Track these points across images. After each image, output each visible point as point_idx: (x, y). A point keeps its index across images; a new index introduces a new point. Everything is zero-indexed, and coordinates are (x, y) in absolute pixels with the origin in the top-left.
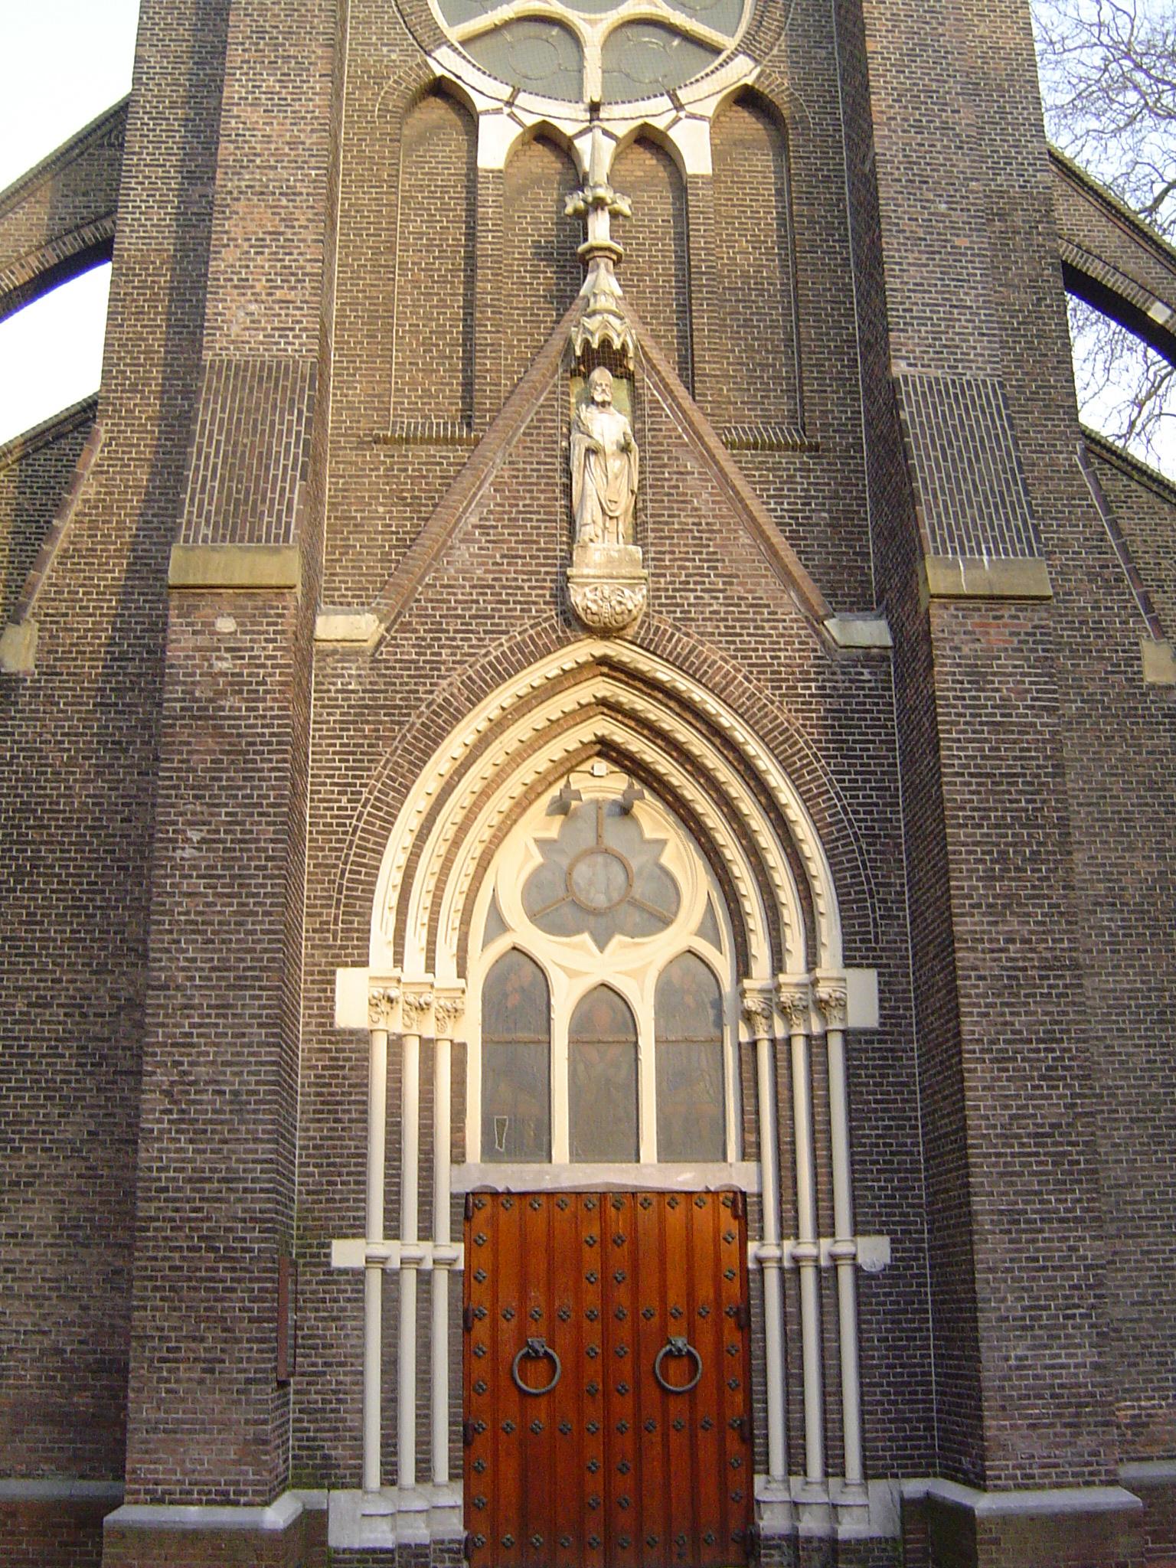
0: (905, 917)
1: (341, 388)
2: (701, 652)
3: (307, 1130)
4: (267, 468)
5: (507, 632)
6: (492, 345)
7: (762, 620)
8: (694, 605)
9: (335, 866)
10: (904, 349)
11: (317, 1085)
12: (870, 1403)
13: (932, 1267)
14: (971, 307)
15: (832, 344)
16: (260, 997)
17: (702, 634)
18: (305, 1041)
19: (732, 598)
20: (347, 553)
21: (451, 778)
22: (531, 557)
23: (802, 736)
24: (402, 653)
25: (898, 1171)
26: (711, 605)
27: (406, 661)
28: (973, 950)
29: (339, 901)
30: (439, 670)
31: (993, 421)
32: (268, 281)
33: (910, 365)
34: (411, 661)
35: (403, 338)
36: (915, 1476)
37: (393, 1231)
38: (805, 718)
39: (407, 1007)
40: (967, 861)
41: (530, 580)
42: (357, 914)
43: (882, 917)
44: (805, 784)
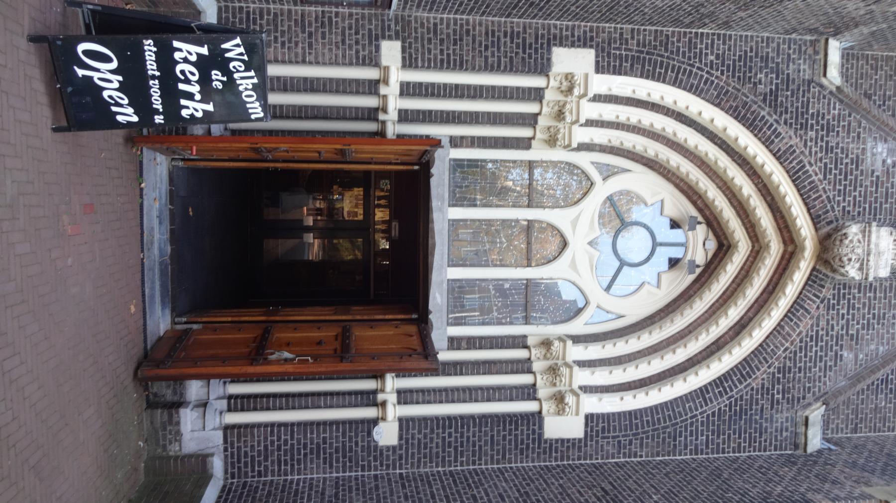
0: (619, 458)
2: (806, 318)
3: (480, 25)
5: (825, 178)
7: (826, 361)
8: (838, 314)
11: (512, 32)
12: (279, 431)
13: (376, 476)
17: (818, 318)
18: (543, 25)
19: (842, 340)
20: (872, 69)
21: (720, 138)
22: (876, 198)
23: (745, 387)
24: (814, 103)
25: (444, 451)
26: (838, 325)
29: (642, 52)
30: (801, 129)
36: (226, 463)
37: (407, 90)
39: (561, 104)
41: (860, 196)
42: (632, 65)
43: (619, 442)
44: (713, 390)
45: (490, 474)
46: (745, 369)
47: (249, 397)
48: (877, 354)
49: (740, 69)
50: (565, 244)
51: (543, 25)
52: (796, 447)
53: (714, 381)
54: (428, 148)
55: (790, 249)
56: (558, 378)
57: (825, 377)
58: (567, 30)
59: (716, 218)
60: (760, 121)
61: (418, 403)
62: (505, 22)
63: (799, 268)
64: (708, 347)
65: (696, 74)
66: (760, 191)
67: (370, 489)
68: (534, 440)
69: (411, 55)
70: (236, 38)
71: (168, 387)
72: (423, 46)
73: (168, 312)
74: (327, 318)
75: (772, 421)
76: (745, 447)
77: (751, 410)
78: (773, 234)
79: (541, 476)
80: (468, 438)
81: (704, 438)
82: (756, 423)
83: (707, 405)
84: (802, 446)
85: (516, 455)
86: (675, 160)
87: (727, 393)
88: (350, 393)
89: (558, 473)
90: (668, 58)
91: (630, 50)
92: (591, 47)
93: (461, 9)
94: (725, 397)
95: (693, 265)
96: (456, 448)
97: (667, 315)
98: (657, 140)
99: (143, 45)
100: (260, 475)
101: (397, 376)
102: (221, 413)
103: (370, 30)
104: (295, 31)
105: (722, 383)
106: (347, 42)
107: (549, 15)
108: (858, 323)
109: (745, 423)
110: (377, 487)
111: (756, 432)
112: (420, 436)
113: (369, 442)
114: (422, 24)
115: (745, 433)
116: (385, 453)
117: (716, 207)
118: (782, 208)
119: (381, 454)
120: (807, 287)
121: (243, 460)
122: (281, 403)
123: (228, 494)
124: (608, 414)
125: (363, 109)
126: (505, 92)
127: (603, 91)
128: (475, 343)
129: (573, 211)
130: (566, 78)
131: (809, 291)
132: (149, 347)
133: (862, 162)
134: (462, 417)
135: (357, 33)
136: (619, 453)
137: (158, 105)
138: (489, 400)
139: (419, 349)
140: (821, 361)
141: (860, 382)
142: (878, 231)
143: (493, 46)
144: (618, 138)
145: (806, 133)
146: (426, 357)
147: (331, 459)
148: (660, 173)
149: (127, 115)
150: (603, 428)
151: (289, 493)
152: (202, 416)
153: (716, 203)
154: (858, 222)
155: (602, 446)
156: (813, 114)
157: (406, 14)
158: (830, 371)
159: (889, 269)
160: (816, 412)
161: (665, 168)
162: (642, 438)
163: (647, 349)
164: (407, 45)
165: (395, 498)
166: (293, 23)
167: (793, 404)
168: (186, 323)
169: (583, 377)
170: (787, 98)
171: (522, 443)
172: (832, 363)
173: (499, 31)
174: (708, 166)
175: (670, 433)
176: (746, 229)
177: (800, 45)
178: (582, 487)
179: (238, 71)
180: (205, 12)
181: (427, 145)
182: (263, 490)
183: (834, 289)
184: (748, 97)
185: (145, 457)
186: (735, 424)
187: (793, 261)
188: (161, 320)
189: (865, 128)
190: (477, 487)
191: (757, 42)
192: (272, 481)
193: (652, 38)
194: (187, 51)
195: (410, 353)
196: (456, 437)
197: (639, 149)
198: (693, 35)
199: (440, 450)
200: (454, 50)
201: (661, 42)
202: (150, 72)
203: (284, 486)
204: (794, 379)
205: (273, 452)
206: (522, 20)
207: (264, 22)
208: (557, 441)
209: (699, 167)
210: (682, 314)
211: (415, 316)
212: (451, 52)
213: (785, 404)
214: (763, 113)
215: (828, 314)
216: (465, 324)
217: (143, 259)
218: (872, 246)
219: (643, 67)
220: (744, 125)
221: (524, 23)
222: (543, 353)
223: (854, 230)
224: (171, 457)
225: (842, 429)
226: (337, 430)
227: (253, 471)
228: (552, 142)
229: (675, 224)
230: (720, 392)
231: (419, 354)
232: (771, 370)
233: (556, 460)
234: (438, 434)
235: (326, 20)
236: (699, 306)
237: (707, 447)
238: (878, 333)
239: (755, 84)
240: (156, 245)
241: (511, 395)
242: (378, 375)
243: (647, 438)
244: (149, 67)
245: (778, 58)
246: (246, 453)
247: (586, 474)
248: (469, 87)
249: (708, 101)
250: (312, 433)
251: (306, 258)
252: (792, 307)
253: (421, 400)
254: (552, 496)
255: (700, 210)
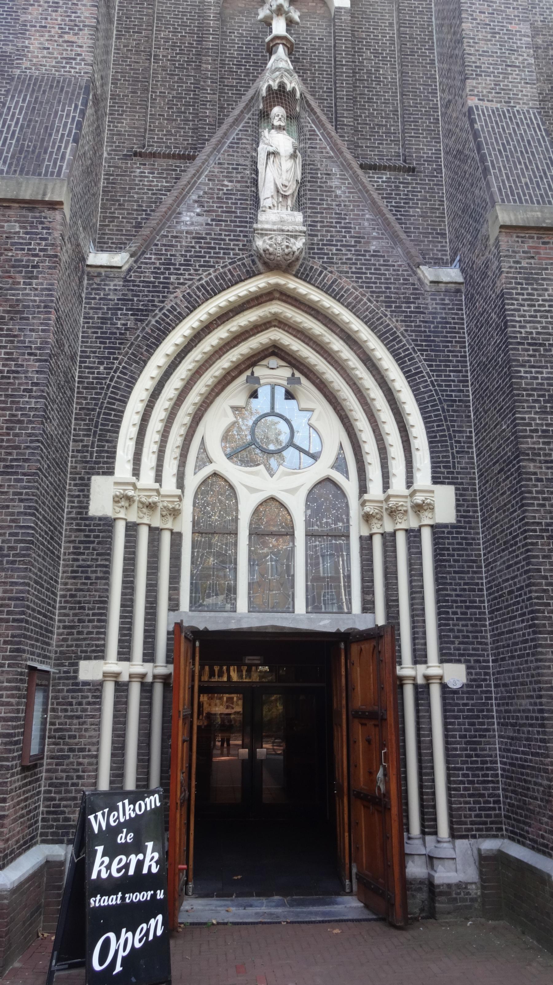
0: (472, 452)
1: (113, 122)
2: (340, 283)
3: (66, 584)
4: (50, 135)
5: (214, 267)
6: (210, 101)
7: (380, 265)
8: (336, 254)
9: (94, 410)
10: (476, 90)
11: (74, 553)
12: (455, 782)
13: (496, 686)
14: (519, 67)
15: (423, 110)
16: (21, 480)
17: (341, 272)
18: (68, 524)
19: (360, 251)
20: (113, 221)
21: (175, 359)
22: (231, 221)
23: (405, 337)
24: (144, 277)
25: (470, 619)
26: (346, 255)
27: (147, 282)
28: (533, 461)
29: (95, 432)
30: (168, 288)
31: (535, 132)
32: (60, 28)
33: (479, 100)
34: (150, 282)
35: (155, 99)
36: (487, 837)
37: (125, 654)
38: (408, 326)
39: (141, 506)
40: (527, 401)
41: (229, 235)
42: (107, 441)
43: (458, 452)
44: (407, 366)
45: (491, 575)
46: (387, 338)
47: (422, 813)
48: (373, 220)
49: (113, 343)
50: (273, 499)
51: (68, 524)
52: (458, 291)
53: (399, 365)
54: (183, 635)
55: (277, 295)
56: (400, 508)
57: (394, 266)
58: (73, 502)
59: (248, 359)
60: (160, 324)
61: (425, 644)
62: (64, 560)
63: (295, 289)
64: (368, 369)
65: (116, 382)
66: (224, 322)
67: (507, 692)
68: (458, 533)
69: (93, 651)
70: (89, 820)
71: (414, 896)
72: (85, 639)
73: (340, 899)
74: (345, 733)
75: (435, 313)
76: (459, 337)
77: (425, 332)
78: (263, 309)
79: (491, 527)
80: (457, 596)
81: (452, 374)
82: (437, 327)
83: (421, 372)
84: (458, 286)
85: (472, 550)
86: (194, 398)
87: (411, 354)
88: (417, 712)
89: (488, 512)
90: (101, 408)
91: (93, 443)
92: (89, 479)
93: (52, 603)
94: (415, 355)
95: (292, 380)
96: (468, 607)
97: (339, 403)
98: (175, 415)
99: (95, 907)
100: (498, 802)
101: (400, 664)
102: (439, 842)
103: (68, 691)
104: (67, 765)
105: (401, 358)
106: (79, 713)
107: (60, 519)
108: (345, 237)
109: (438, 337)
110: (505, 685)
111: (446, 328)
112: (457, 642)
113: (463, 693)
114: (64, 640)
115: (447, 337)
116: (473, 677)
117: (238, 359)
118: (240, 303)
119: (474, 680)
120: (312, 282)
121: (484, 819)
122: (428, 781)
123: (516, 833)
124: (432, 463)
125: (142, 697)
126: (129, 559)
127: (129, 467)
128: (368, 587)
129: (241, 492)
130: (118, 502)
131: (316, 280)
132: (375, 917)
133: (199, 233)
134: (438, 601)
135: (71, 704)
136: (468, 453)
137: (147, 895)
138: (421, 575)
139: (373, 643)
140: (380, 270)
141: (398, 236)
142: (262, 222)
143: (87, 572)
144: (172, 451)
145: (172, 284)
146: (381, 637)
147: (481, 730)
148: (206, 410)
149: (156, 925)
150: (445, 467)
151: (513, 772)
152: (442, 861)
153: (234, 359)
154: (254, 237)
155: (461, 468)
156: (154, 277)
157: (53, 655)
158: (388, 261)
159: (296, 213)
160: (427, 274)
161: (201, 406)
162: (454, 431)
163: (371, 424)
164: (83, 655)
165: (513, 668)
166: (60, 768)
167: (419, 294)
168: (351, 881)
169: (398, 484)
170: (140, 301)
171: (461, 544)
172: (382, 259)
173: (72, 567)
174: (200, 368)
175: (448, 406)
176: (259, 332)
177: (92, 289)
178: (498, 491)
179: (118, 818)
180: (47, 856)
181: (180, 636)
182: (511, 798)
183: (314, 258)
184: (138, 336)
185: (483, 920)
186: (439, 346)
187: (288, 293)
188: (348, 906)
189: (168, 232)
190: (502, 589)
191: (88, 328)
192: (503, 789)
193: (83, 422)
194: (101, 867)
195: (377, 652)
196: (457, 607)
197: (183, 431)
198: (81, 386)
199: (469, 623)
200: (89, 609)
201: (86, 415)
202: (119, 902)
203: (507, 777)
204: (396, 293)
205: (475, 789)
206: (63, 544)
207: (58, 796)
208: (458, 511)
209: (201, 376)
210: (339, 391)
211: (342, 646)
212: (91, 612)
213: (420, 301)
214: (153, 322)
215: (336, 263)
216: (349, 571)
217: (287, 923)
218: (275, 227)
219: (109, 431)
220: (164, 339)
221: (66, 542)
222: (376, 521)
223: (260, 243)
224: (482, 893)
225: (442, 246)
226: (452, 724)
227: (494, 809)
228: (175, 513)
229: (254, 395)
230: (409, 360)
231: (378, 644)
232: (388, 314)
233: (476, 512)
234: (454, 625)
235: (57, 734)
236: (331, 375)
237: (460, 371)
238: (353, 219)
239: (126, 329)
240: (273, 910)
241: (416, 553)
242: (399, 683)
243: (453, 426)
244: (114, 903)
245: (103, 309)
246: (477, 816)
247: (487, 485)
248: (123, 594)
249: (141, 372)
250: (456, 749)
251: (281, 757)
252: (330, 295)
253: (422, 641)
254: (506, 520)
255: (241, 373)
